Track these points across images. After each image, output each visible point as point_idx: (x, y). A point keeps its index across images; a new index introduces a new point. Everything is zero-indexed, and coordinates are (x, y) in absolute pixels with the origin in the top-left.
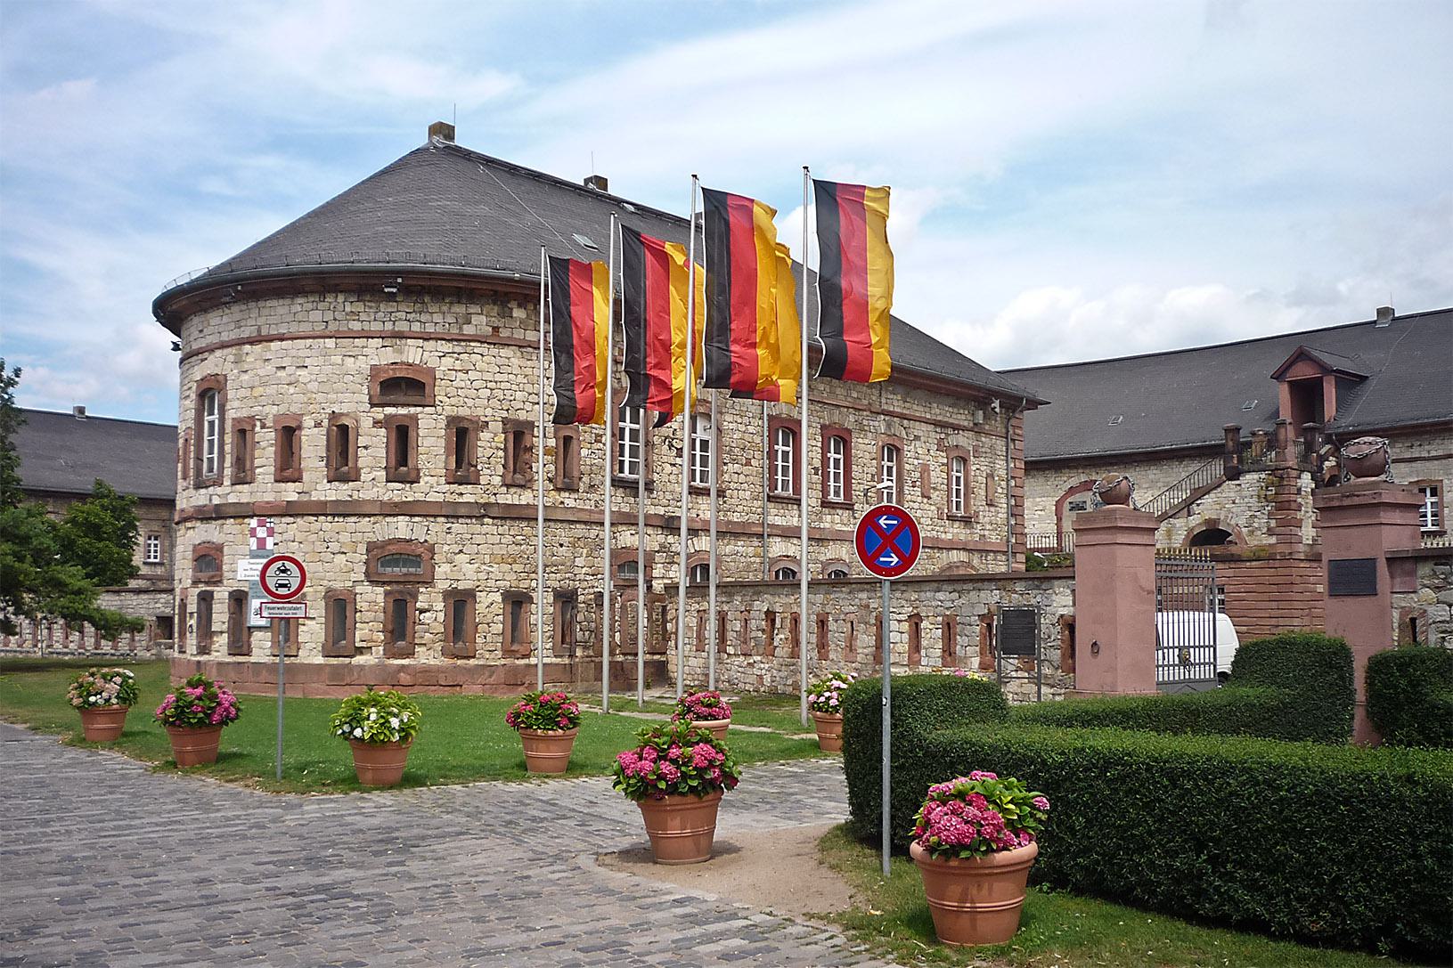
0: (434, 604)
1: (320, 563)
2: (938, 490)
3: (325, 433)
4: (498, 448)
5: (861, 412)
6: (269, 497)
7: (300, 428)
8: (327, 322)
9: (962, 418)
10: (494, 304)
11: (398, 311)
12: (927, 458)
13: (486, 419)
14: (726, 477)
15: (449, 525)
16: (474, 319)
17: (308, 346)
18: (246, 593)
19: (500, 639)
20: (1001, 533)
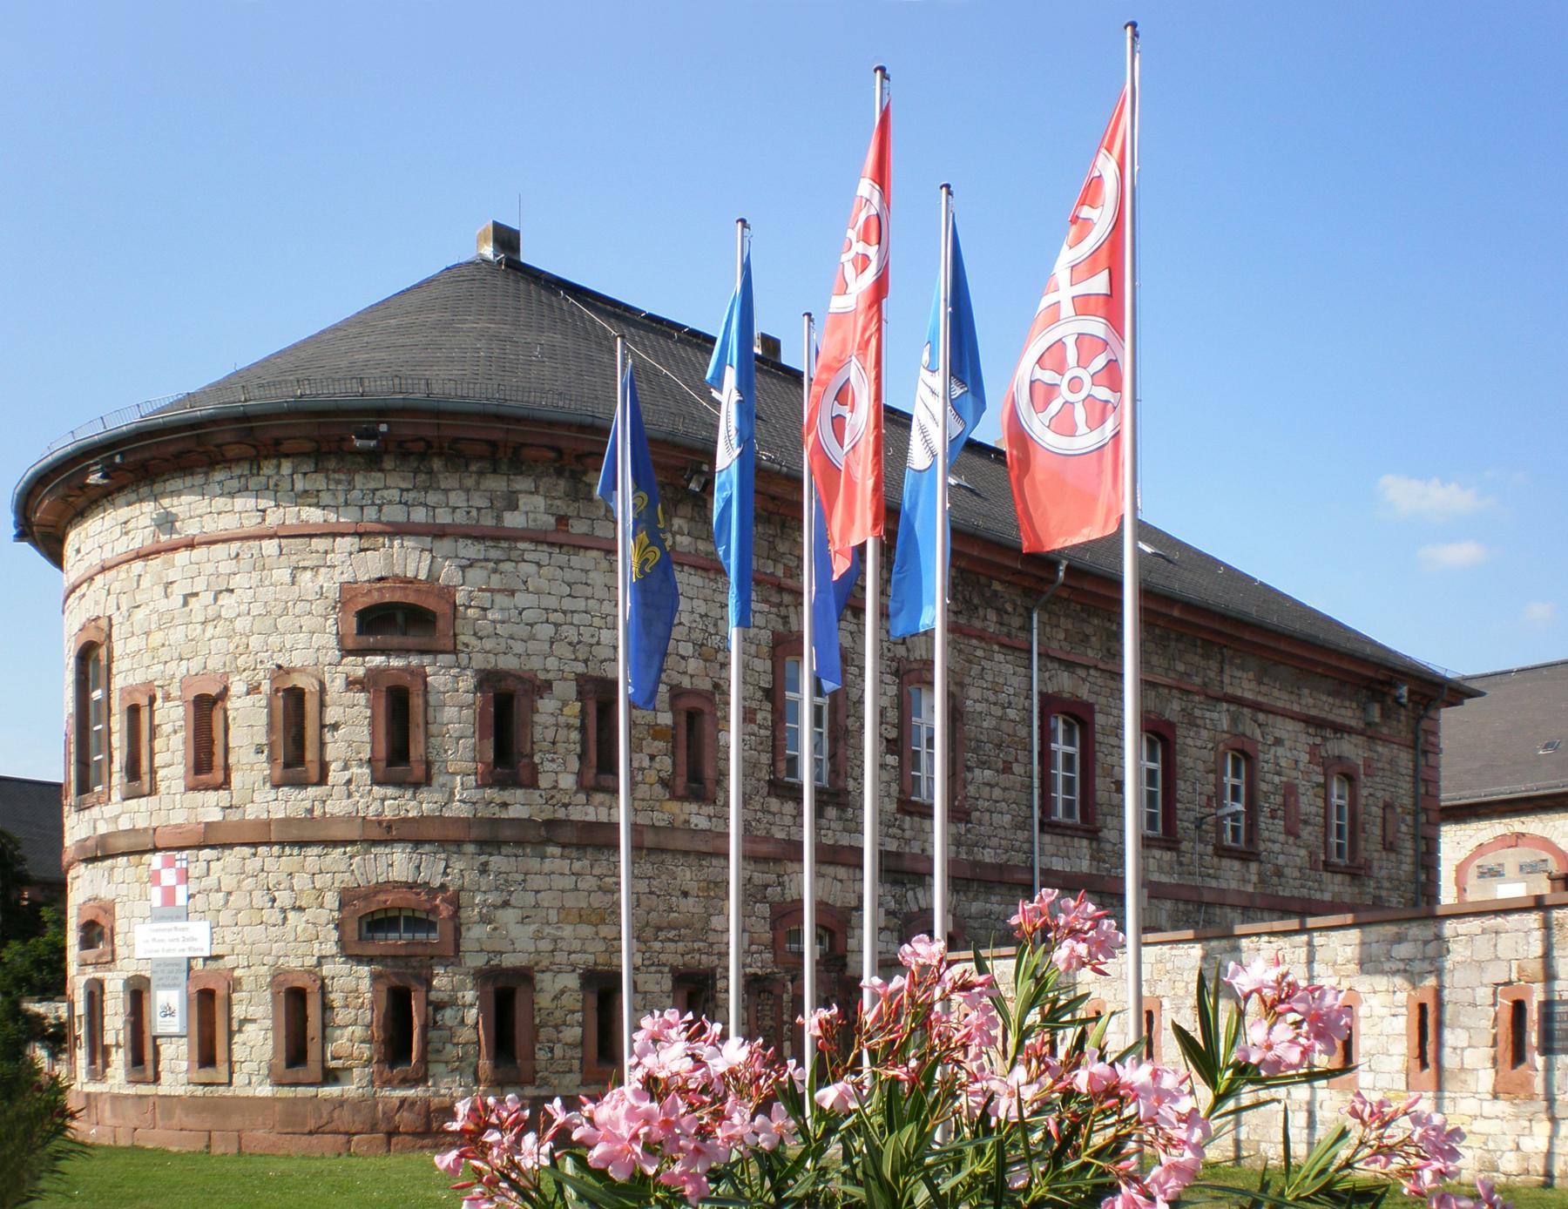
0: (460, 995)
1: (263, 926)
2: (1310, 824)
3: (264, 703)
4: (569, 726)
5: (1191, 697)
6: (178, 818)
7: (224, 694)
8: (264, 511)
9: (1347, 714)
10: (559, 473)
11: (386, 488)
12: (1294, 774)
13: (550, 676)
14: (972, 790)
15: (483, 858)
16: (523, 501)
17: (233, 555)
18: (148, 980)
19: (578, 1053)
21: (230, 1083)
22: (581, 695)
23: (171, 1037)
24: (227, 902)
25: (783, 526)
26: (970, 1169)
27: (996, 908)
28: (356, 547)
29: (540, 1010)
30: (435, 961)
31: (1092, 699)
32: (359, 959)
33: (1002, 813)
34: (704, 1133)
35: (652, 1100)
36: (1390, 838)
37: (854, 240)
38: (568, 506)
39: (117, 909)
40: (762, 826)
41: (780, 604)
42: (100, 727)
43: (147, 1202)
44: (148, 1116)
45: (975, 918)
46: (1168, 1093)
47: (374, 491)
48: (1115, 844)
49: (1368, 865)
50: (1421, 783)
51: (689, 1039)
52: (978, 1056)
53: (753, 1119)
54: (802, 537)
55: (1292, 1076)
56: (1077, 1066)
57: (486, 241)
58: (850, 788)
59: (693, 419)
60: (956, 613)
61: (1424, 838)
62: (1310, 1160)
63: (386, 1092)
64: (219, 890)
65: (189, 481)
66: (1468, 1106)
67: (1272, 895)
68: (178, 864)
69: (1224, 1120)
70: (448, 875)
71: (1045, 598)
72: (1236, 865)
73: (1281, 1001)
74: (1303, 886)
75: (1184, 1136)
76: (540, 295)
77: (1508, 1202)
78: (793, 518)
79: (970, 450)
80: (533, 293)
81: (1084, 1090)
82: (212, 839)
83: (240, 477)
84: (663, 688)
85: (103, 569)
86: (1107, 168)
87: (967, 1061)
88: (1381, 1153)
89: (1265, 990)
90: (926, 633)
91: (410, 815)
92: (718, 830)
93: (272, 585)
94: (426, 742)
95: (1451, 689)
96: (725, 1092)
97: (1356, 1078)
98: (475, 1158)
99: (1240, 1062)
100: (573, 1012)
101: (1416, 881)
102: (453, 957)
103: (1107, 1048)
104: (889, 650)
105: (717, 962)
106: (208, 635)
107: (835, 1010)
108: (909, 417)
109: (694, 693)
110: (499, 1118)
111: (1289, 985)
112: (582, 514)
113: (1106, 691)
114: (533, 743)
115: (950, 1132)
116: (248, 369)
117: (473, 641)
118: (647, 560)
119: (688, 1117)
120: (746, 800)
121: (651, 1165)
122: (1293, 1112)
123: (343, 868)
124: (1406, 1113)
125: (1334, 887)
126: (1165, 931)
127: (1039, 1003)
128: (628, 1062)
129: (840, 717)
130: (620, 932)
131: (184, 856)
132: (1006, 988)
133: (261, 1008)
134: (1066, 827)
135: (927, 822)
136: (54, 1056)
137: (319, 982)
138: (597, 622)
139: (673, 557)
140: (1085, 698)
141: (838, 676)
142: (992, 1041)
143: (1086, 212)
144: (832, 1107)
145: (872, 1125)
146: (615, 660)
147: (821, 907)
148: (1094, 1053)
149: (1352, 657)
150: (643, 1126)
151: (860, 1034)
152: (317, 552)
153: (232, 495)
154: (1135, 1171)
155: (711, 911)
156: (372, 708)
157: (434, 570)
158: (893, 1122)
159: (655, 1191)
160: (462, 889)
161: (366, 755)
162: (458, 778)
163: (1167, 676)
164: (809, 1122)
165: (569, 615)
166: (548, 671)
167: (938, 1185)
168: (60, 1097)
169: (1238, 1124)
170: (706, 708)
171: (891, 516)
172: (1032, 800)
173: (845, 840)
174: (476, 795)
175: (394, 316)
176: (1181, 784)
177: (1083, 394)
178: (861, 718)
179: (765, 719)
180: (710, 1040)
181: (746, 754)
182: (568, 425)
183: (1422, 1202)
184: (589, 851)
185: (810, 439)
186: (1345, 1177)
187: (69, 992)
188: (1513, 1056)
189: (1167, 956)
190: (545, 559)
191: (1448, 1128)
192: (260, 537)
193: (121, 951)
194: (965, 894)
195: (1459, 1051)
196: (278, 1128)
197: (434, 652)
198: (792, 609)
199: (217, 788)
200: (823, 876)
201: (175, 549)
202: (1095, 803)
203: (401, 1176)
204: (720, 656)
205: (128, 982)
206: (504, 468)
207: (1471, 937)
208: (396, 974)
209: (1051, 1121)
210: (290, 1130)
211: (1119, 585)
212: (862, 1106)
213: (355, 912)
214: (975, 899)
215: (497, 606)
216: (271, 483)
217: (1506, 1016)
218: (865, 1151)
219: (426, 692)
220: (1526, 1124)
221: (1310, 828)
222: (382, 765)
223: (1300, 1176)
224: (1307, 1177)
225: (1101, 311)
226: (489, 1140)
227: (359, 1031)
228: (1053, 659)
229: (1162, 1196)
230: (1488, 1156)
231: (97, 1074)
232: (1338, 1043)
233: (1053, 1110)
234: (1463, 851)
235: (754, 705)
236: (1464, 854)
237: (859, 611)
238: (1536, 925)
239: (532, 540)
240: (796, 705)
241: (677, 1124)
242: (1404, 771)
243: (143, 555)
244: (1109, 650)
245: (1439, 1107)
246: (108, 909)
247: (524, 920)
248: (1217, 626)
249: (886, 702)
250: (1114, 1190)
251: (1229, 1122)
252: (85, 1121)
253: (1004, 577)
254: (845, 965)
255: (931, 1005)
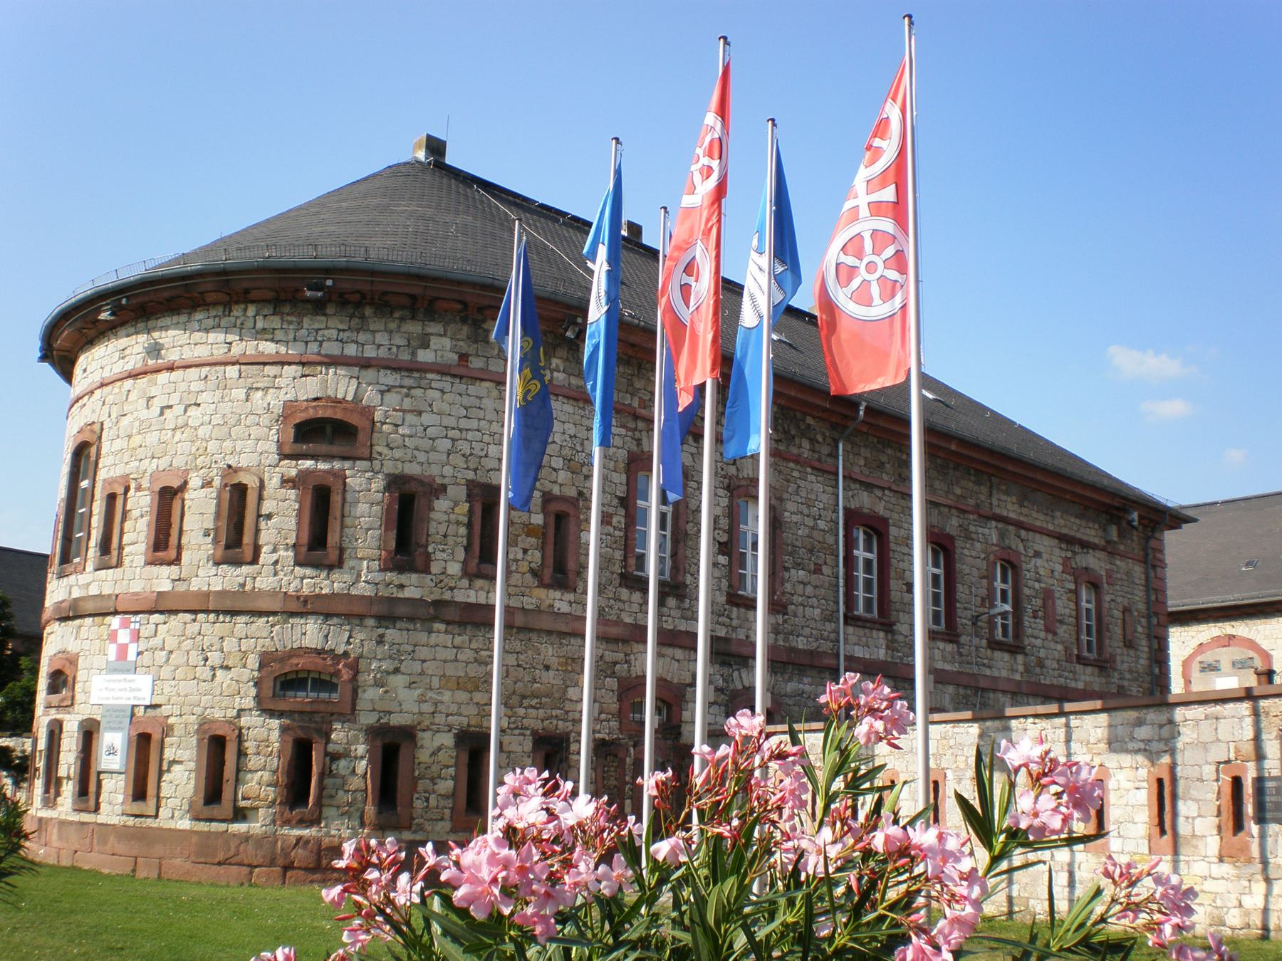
0: (353, 748)
1: (195, 681)
2: (1065, 624)
3: (214, 495)
4: (458, 523)
6: (136, 587)
7: (183, 487)
8: (230, 343)
9: (1091, 533)
11: (327, 328)
12: (1051, 581)
13: (446, 481)
14: (788, 587)
15: (381, 631)
16: (435, 342)
17: (203, 376)
18: (99, 723)
19: (449, 803)
20: (1144, 685)
21: (156, 816)
22: (470, 497)
23: (112, 773)
24: (168, 659)
25: (639, 367)
26: (783, 919)
27: (807, 688)
28: (299, 374)
29: (419, 764)
30: (335, 716)
31: (886, 514)
32: (272, 713)
33: (813, 607)
34: (554, 879)
35: (510, 848)
36: (1129, 637)
37: (701, 156)
38: (469, 346)
39: (80, 661)
40: (614, 612)
41: (635, 430)
42: (83, 510)
43: (79, 917)
44: (88, 840)
45: (790, 697)
46: (952, 854)
47: (317, 330)
48: (906, 637)
49: (1112, 659)
50: (1152, 592)
51: (544, 795)
52: (791, 817)
53: (596, 868)
54: (655, 377)
55: (1055, 841)
56: (875, 828)
57: (420, 148)
58: (688, 582)
59: (572, 283)
60: (777, 441)
61: (1156, 637)
62: (1071, 916)
63: (285, 831)
64: (163, 649)
65: (175, 319)
66: (1199, 868)
67: (1035, 683)
68: (132, 626)
69: (999, 878)
70: (350, 644)
71: (848, 431)
72: (1006, 656)
73: (1045, 775)
74: (1060, 676)
75: (965, 893)
76: (458, 187)
77: (1234, 953)
78: (648, 362)
79: (788, 314)
80: (453, 187)
81: (881, 850)
82: (162, 606)
83: (215, 317)
84: (537, 494)
85: (102, 385)
86: (893, 112)
87: (781, 821)
88: (1130, 910)
89: (1031, 765)
90: (752, 456)
91: (323, 592)
92: (577, 614)
93: (230, 401)
94: (342, 531)
95: (1171, 516)
96: (574, 843)
97: (1107, 844)
98: (356, 893)
99: (1011, 828)
100: (447, 767)
101: (1151, 673)
102: (349, 715)
103: (900, 813)
104: (722, 469)
105: (571, 728)
106: (176, 439)
107: (670, 773)
108: (742, 287)
109: (562, 499)
110: (379, 858)
111: (1051, 760)
112: (480, 353)
113: (898, 508)
114: (428, 535)
115: (766, 885)
116: (230, 236)
117: (385, 451)
118: (529, 390)
119: (540, 864)
120: (601, 589)
121: (507, 906)
122: (1056, 872)
123: (265, 634)
124: (1149, 874)
125: (1085, 677)
126: (948, 711)
127: (843, 772)
128: (492, 813)
129: (681, 522)
130: (491, 699)
131: (138, 619)
132: (815, 758)
133: (188, 752)
134: (867, 620)
135: (751, 613)
136: (17, 784)
137: (237, 732)
138: (486, 439)
139: (550, 389)
140: (881, 513)
141: (681, 490)
142: (803, 804)
143: (877, 142)
144: (665, 859)
145: (699, 876)
146: (499, 470)
147: (661, 683)
148: (889, 817)
149: (1094, 487)
150: (502, 871)
151: (691, 795)
152: (269, 376)
153: (207, 330)
154: (924, 923)
155: (568, 683)
156: (300, 502)
157: (359, 393)
158: (716, 876)
159: (510, 930)
160: (361, 656)
161: (292, 541)
162: (365, 563)
163: (947, 498)
164: (644, 872)
165: (464, 432)
166: (444, 477)
167: (755, 932)
168: (18, 820)
169: (1010, 883)
170: (571, 511)
171: (725, 362)
172: (838, 597)
173: (683, 626)
174: (378, 577)
175: (345, 200)
176: (959, 587)
177: (877, 275)
178: (699, 524)
179: (619, 522)
180: (562, 796)
181: (603, 550)
182: (474, 285)
183: (1164, 953)
184: (469, 627)
185: (663, 301)
186: (1101, 930)
187: (34, 730)
188: (1234, 825)
189: (950, 733)
190: (447, 387)
191: (1184, 887)
192: (225, 364)
193: (79, 697)
194: (782, 675)
195: (1190, 820)
196: (193, 858)
197: (354, 459)
198: (644, 433)
199: (170, 564)
200: (663, 656)
201: (158, 371)
202: (890, 601)
203: (293, 906)
204: (585, 470)
205: (82, 723)
206: (421, 316)
207: (1197, 722)
208: (301, 728)
209: (852, 876)
210: (202, 860)
211: (907, 423)
212: (690, 859)
213: (272, 672)
214: (790, 680)
215: (407, 423)
216: (239, 322)
217: (1227, 790)
218: (692, 900)
219: (344, 491)
220: (1247, 884)
221: (1065, 627)
222: (304, 549)
223: (1063, 930)
224: (1069, 930)
225: (890, 214)
226: (369, 877)
227: (266, 776)
228: (855, 481)
229: (947, 946)
230: (1216, 912)
231: (49, 803)
232: (1093, 812)
233: (854, 867)
234: (1187, 649)
235: (611, 510)
236: (1188, 651)
237: (699, 437)
238: (1247, 713)
239: (438, 372)
240: (645, 511)
241: (531, 870)
242: (1138, 582)
243: (133, 375)
244: (900, 475)
245: (1176, 870)
246: (73, 661)
247: (411, 685)
248: (986, 458)
249: (719, 511)
250: (906, 940)
251: (1002, 881)
252: (36, 842)
253: (815, 413)
254: (679, 734)
255: (752, 771)
